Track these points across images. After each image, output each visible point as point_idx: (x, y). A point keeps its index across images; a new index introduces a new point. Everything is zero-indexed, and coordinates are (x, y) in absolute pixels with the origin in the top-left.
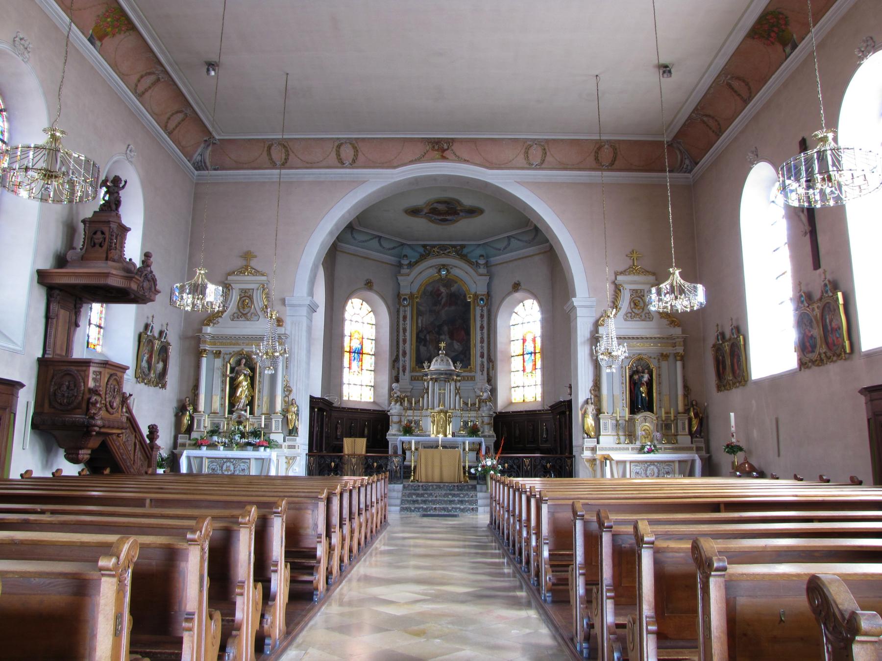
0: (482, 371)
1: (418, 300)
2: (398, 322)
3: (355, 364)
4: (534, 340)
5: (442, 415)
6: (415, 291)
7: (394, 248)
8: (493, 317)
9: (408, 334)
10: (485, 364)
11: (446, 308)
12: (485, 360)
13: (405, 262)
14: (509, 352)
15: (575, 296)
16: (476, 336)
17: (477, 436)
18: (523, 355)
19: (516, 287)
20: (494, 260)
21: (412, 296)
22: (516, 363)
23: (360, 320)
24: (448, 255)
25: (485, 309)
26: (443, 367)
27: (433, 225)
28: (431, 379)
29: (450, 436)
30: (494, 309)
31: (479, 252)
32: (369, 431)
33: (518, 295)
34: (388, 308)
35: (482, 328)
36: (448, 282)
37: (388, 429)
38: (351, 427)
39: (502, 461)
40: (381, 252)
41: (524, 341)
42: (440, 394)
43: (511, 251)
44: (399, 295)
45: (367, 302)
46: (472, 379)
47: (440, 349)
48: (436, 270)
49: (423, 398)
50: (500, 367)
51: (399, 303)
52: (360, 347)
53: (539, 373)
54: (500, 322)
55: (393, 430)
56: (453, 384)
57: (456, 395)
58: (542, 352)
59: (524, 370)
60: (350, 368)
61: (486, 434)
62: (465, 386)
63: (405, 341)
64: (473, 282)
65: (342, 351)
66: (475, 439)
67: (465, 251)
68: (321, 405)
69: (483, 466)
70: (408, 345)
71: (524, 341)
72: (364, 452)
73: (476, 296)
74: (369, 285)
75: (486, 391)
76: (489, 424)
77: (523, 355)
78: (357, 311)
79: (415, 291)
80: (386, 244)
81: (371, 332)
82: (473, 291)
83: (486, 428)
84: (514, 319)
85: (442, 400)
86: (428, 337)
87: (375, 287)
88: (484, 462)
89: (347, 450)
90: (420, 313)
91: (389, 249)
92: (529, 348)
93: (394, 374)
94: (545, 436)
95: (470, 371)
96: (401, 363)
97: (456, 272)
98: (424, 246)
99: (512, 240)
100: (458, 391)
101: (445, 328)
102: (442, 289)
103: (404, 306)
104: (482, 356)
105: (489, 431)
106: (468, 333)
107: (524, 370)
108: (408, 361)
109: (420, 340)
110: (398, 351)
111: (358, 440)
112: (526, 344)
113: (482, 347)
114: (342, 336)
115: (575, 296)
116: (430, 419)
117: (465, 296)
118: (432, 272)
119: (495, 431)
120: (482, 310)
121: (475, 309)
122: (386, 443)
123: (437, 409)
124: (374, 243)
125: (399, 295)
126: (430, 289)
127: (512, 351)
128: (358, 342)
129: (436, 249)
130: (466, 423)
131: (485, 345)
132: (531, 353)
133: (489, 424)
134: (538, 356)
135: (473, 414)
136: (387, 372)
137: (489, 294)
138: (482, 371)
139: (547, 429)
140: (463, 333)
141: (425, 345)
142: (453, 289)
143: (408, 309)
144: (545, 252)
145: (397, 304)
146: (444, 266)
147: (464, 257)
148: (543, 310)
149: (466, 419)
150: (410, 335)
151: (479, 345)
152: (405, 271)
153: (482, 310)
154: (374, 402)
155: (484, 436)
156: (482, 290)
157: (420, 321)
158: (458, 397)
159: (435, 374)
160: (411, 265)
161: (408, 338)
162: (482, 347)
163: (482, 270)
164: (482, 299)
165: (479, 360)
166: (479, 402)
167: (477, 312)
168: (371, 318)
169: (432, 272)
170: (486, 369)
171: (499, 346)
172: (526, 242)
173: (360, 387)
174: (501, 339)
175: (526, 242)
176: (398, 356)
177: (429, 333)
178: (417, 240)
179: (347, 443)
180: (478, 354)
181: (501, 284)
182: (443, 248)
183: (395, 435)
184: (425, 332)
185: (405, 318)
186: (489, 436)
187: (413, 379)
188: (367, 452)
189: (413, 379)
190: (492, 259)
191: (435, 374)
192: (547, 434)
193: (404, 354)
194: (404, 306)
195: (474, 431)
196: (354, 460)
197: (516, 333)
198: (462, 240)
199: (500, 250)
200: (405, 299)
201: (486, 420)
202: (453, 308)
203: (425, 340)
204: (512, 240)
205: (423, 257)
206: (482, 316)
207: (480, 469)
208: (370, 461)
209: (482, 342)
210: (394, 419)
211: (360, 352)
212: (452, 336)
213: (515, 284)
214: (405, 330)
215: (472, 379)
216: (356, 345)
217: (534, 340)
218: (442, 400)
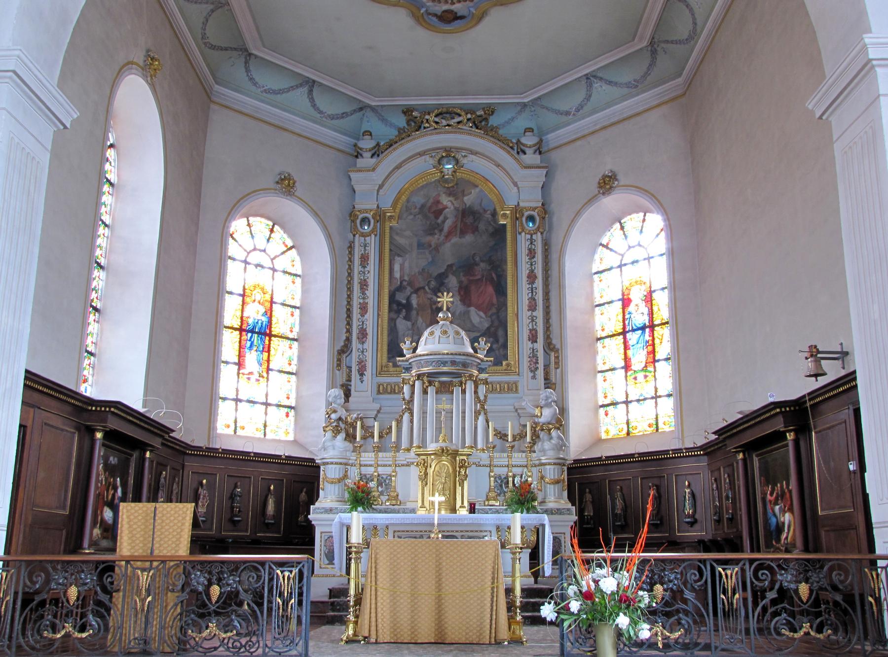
0: (534, 370)
1: (394, 223)
2: (350, 268)
3: (251, 358)
4: (649, 299)
5: (446, 462)
6: (386, 204)
7: (344, 115)
8: (554, 256)
9: (371, 293)
10: (541, 354)
11: (455, 240)
12: (540, 345)
13: (367, 144)
14: (592, 329)
15: (869, 31)
16: (520, 295)
17: (533, 510)
18: (624, 333)
19: (607, 184)
20: (552, 138)
21: (380, 216)
22: (610, 353)
23: (267, 263)
24: (456, 128)
25: (538, 237)
26: (446, 347)
27: (422, 34)
28: (419, 377)
29: (463, 512)
30: (556, 238)
31: (522, 122)
32: (278, 504)
33: (610, 202)
34: (329, 237)
35: (532, 277)
36: (456, 187)
37: (313, 496)
38: (232, 497)
39: (650, 576)
40: (315, 122)
41: (626, 302)
42: (438, 413)
43: (594, 112)
44: (352, 215)
45: (282, 227)
46: (512, 388)
47: (440, 309)
48: (432, 162)
49: (399, 422)
50: (572, 358)
51: (354, 231)
52: (265, 319)
53: (664, 370)
54: (571, 264)
55: (328, 497)
56: (470, 387)
57: (477, 414)
58: (676, 322)
59: (627, 367)
60: (240, 364)
61: (551, 505)
62: (497, 403)
63: (364, 309)
64: (506, 180)
65: (217, 326)
66: (533, 519)
67: (494, 121)
68: (114, 424)
69: (587, 596)
70: (370, 316)
71: (626, 302)
72: (183, 549)
73: (517, 212)
74: (286, 185)
75: (548, 405)
76: (557, 482)
77: (624, 333)
78: (261, 243)
79: (386, 204)
80: (323, 102)
81: (288, 291)
82: (512, 203)
83: (551, 490)
84: (603, 259)
85: (443, 423)
86: (414, 302)
87: (299, 190)
88: (587, 583)
89: (128, 544)
90: (397, 251)
91: (333, 117)
92: (639, 317)
93: (341, 378)
94: (689, 510)
95: (508, 371)
96: (355, 355)
97: (473, 163)
98: (407, 111)
99: (597, 85)
100: (481, 408)
101: (452, 281)
102: (445, 200)
103: (363, 235)
104: (533, 338)
105: (555, 497)
106: (501, 291)
107: (627, 367)
108: (370, 350)
109: (399, 307)
110: (349, 331)
111: (163, 507)
112: (631, 308)
113: (533, 319)
114: (219, 291)
115: (869, 31)
116: (415, 472)
117: (494, 214)
118: (426, 164)
119: (571, 498)
120: (532, 242)
121: (515, 240)
122: (309, 529)
123: (432, 447)
124: (300, 96)
125: (352, 215)
126: (419, 200)
127: (598, 327)
128: (262, 310)
129: (431, 118)
130: (502, 482)
131: (539, 313)
132: (643, 328)
133: (557, 482)
134: (664, 334)
135: (518, 458)
136: (325, 375)
137: (545, 209)
138: (534, 370)
139: (693, 495)
140: (490, 290)
141: (407, 318)
142: (469, 200)
143: (372, 241)
144: (673, 99)
145: (349, 228)
146: (449, 153)
147: (492, 133)
148: (671, 230)
149: (503, 471)
150: (374, 298)
151: (525, 314)
152: (367, 161)
153: (532, 242)
154: (295, 442)
155: (546, 511)
156: (530, 199)
157: (397, 267)
158: (481, 418)
159: (428, 363)
160: (377, 152)
161: (371, 301)
162: (533, 319)
163: (531, 157)
164: (531, 218)
165: (527, 345)
166: (533, 429)
167: (520, 252)
168: (292, 261)
169: (426, 164)
170: (541, 365)
171: (570, 315)
172: (628, 85)
173: (260, 408)
174: (573, 300)
175: (628, 85)
176: (348, 340)
177: (416, 291)
178: (392, 94)
179: (132, 518)
180: (525, 334)
181: (569, 186)
182: (446, 113)
183: (330, 511)
184: (409, 290)
185: (364, 259)
186: (559, 512)
187: (382, 390)
188: (192, 552)
189: (382, 390)
190: (550, 136)
191: (428, 363)
192: (694, 506)
193: (363, 334)
194: (363, 235)
195: (524, 499)
196: (144, 579)
197: (608, 288)
198: (489, 92)
199: (567, 113)
200: (365, 220)
201: (551, 473)
202: (469, 238)
203: (408, 306)
204: (597, 85)
205: (403, 135)
206: (532, 254)
207: (575, 606)
208: (199, 580)
209: (532, 307)
210: (329, 473)
211: (265, 332)
212: (465, 295)
213: (604, 177)
214: (364, 285)
215: (510, 390)
216: (255, 313)
217: (649, 299)
218: (443, 423)
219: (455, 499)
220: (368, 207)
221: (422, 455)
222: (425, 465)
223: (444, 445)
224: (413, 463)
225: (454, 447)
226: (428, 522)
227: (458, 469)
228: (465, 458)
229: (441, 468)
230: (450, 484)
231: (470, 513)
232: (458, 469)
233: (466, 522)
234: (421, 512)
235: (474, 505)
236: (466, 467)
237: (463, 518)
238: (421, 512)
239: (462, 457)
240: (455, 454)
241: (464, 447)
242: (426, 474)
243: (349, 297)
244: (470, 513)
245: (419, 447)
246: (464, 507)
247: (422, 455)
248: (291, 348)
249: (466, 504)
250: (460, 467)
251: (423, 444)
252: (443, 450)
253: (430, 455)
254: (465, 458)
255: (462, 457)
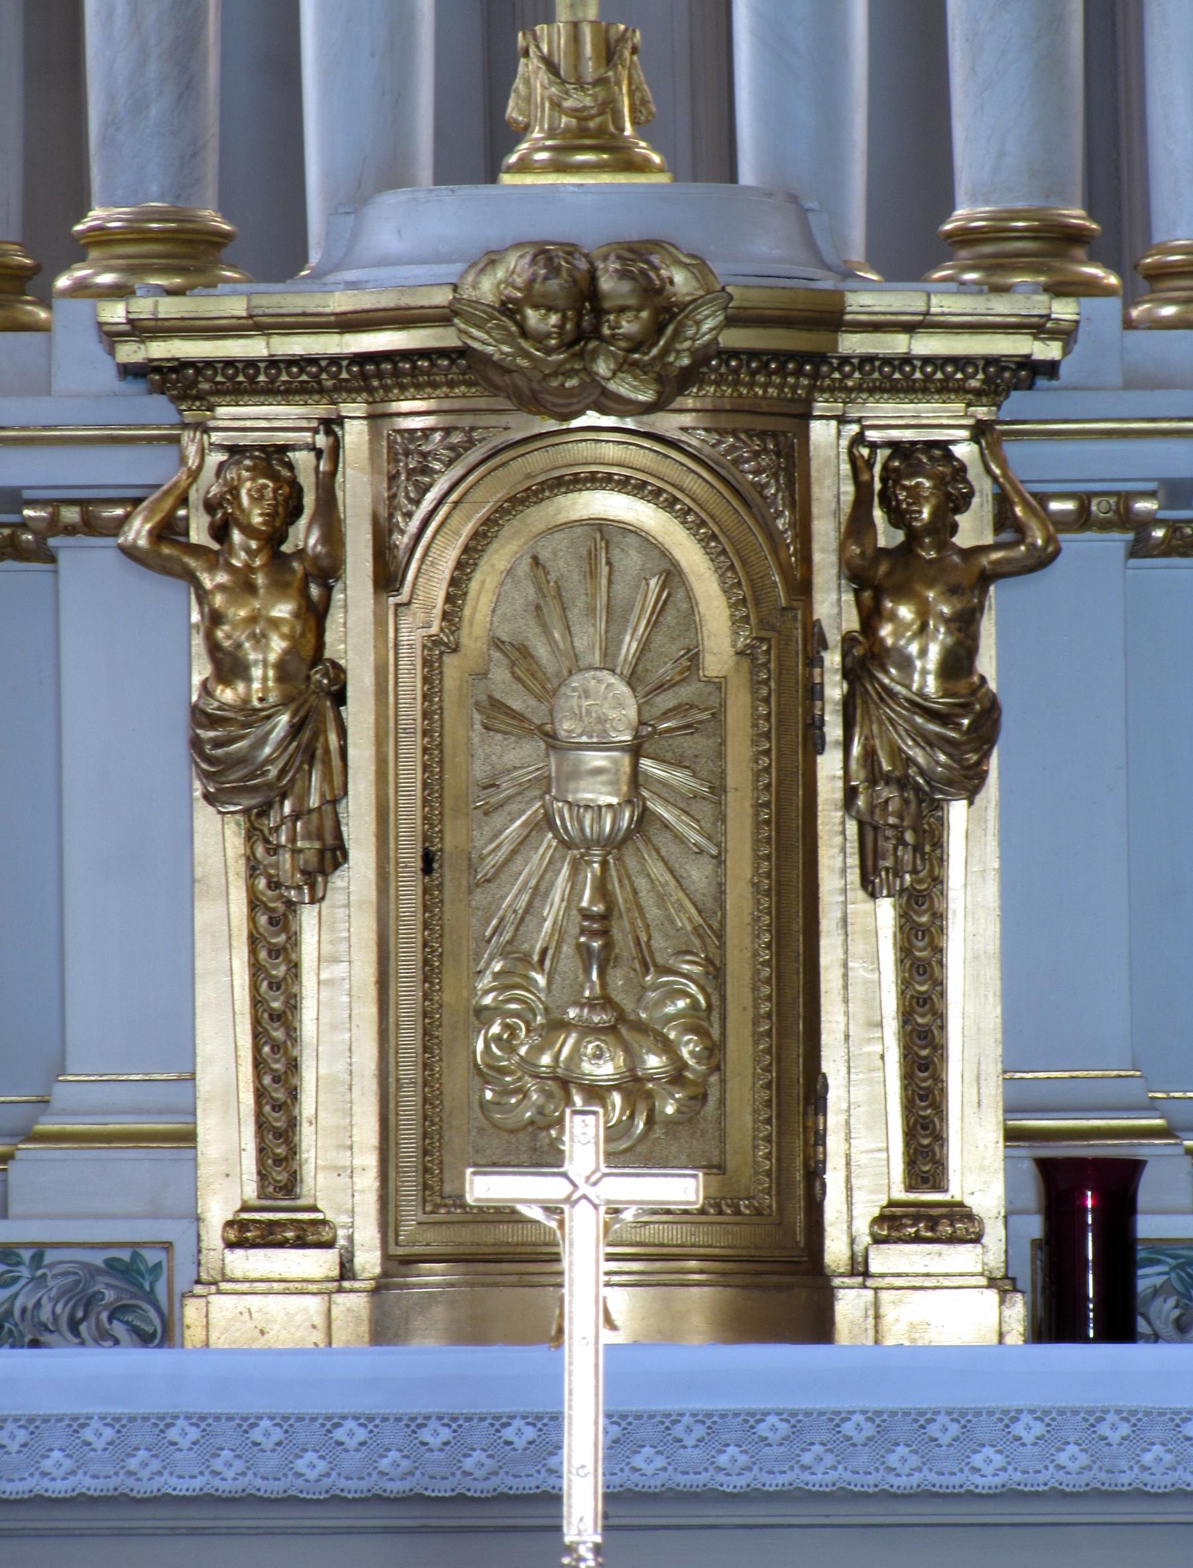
5: (627, 490)
29: (944, 1310)
123: (403, 248)
219: (799, 1095)
220: (838, 820)
221: (244, 379)
222: (280, 539)
223: (558, 197)
224: (93, 519)
225: (759, 254)
226: (477, 1469)
227: (834, 607)
228: (943, 421)
229: (547, 595)
230: (706, 866)
231: (1056, 1321)
232: (834, 607)
233: (989, 1469)
234: (265, 1315)
235: (1118, 1182)
236: (973, 581)
237: (931, 1404)
238: (265, 1315)
239: (896, 419)
240: (785, 361)
241: (915, 235)
242: (314, 687)
243: (692, 817)
244: (1056, 1321)
245: (190, 251)
246: (950, 1224)
247: (244, 379)
248: (897, 1320)
249: (980, 1172)
250: (872, 582)
251: (251, 219)
252: (586, 301)
253: (374, 376)
254: (943, 421)
255: (896, 419)
